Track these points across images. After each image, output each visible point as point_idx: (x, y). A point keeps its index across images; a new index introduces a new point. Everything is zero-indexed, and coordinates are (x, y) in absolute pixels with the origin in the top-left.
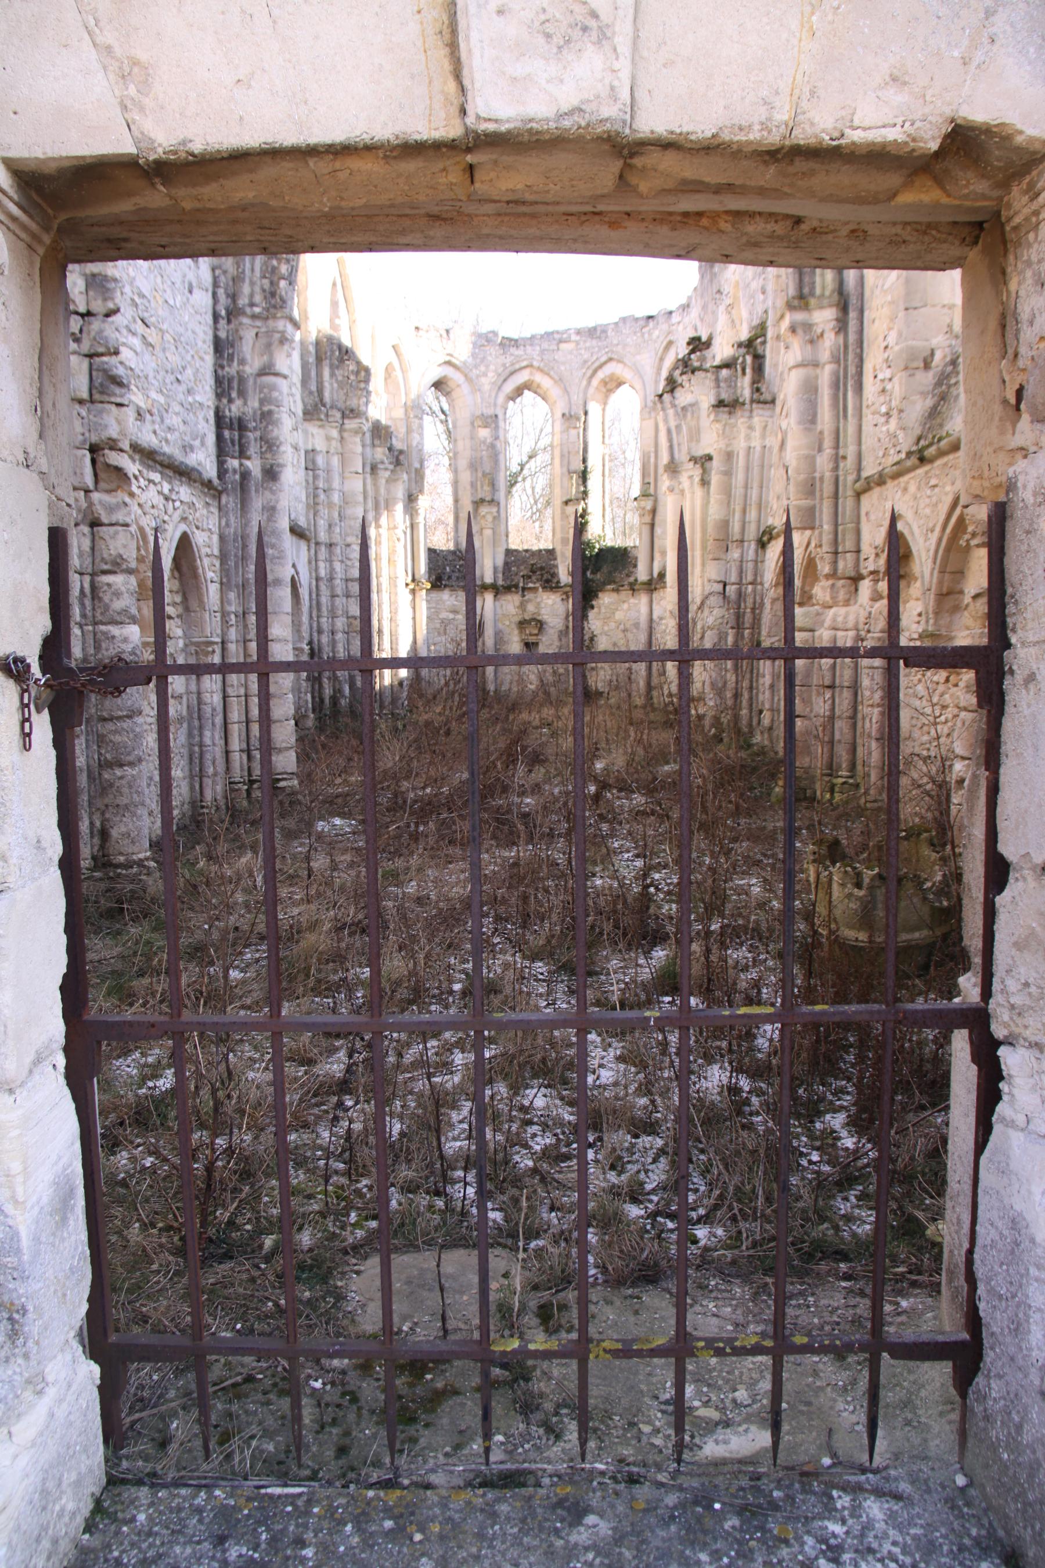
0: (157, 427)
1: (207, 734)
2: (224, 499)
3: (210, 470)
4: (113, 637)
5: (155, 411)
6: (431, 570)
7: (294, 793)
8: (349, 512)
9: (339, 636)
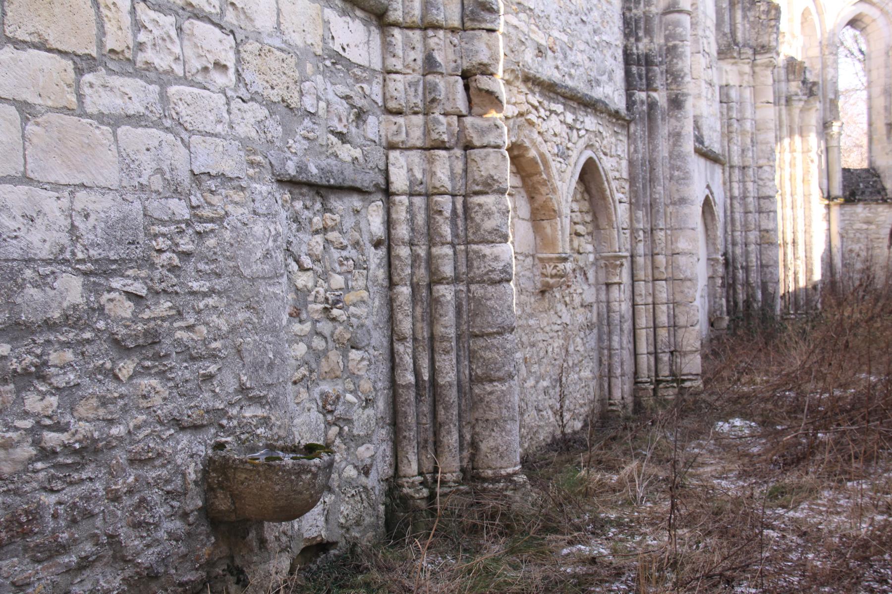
0: (559, 63)
1: (616, 338)
2: (632, 128)
3: (618, 102)
4: (484, 256)
5: (557, 48)
6: (845, 187)
7: (697, 394)
8: (761, 137)
9: (752, 247)
